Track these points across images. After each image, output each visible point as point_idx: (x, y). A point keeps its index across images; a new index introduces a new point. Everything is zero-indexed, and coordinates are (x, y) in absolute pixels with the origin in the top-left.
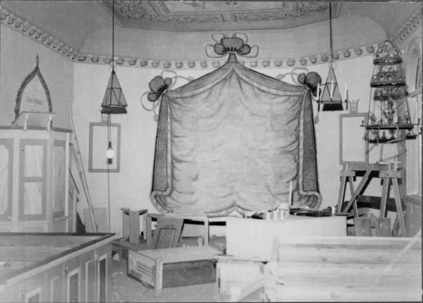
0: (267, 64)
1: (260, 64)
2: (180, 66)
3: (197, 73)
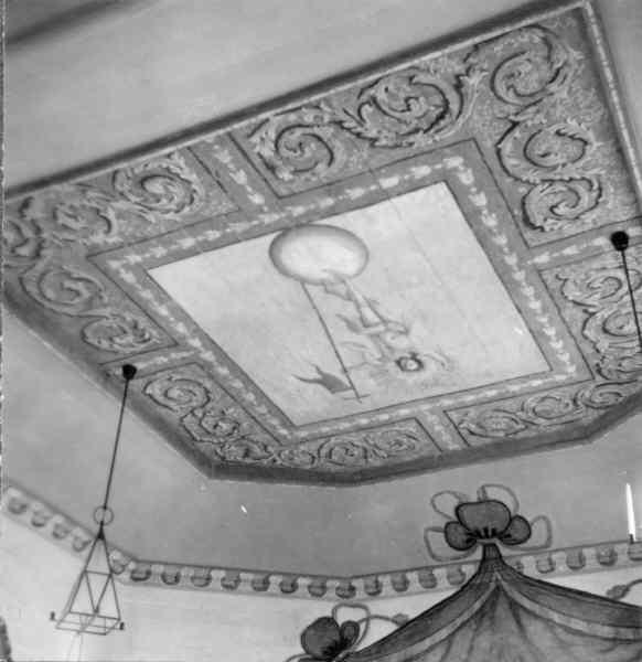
0: (577, 565)
1: (561, 568)
2: (376, 592)
3: (414, 605)
